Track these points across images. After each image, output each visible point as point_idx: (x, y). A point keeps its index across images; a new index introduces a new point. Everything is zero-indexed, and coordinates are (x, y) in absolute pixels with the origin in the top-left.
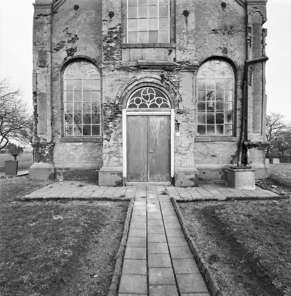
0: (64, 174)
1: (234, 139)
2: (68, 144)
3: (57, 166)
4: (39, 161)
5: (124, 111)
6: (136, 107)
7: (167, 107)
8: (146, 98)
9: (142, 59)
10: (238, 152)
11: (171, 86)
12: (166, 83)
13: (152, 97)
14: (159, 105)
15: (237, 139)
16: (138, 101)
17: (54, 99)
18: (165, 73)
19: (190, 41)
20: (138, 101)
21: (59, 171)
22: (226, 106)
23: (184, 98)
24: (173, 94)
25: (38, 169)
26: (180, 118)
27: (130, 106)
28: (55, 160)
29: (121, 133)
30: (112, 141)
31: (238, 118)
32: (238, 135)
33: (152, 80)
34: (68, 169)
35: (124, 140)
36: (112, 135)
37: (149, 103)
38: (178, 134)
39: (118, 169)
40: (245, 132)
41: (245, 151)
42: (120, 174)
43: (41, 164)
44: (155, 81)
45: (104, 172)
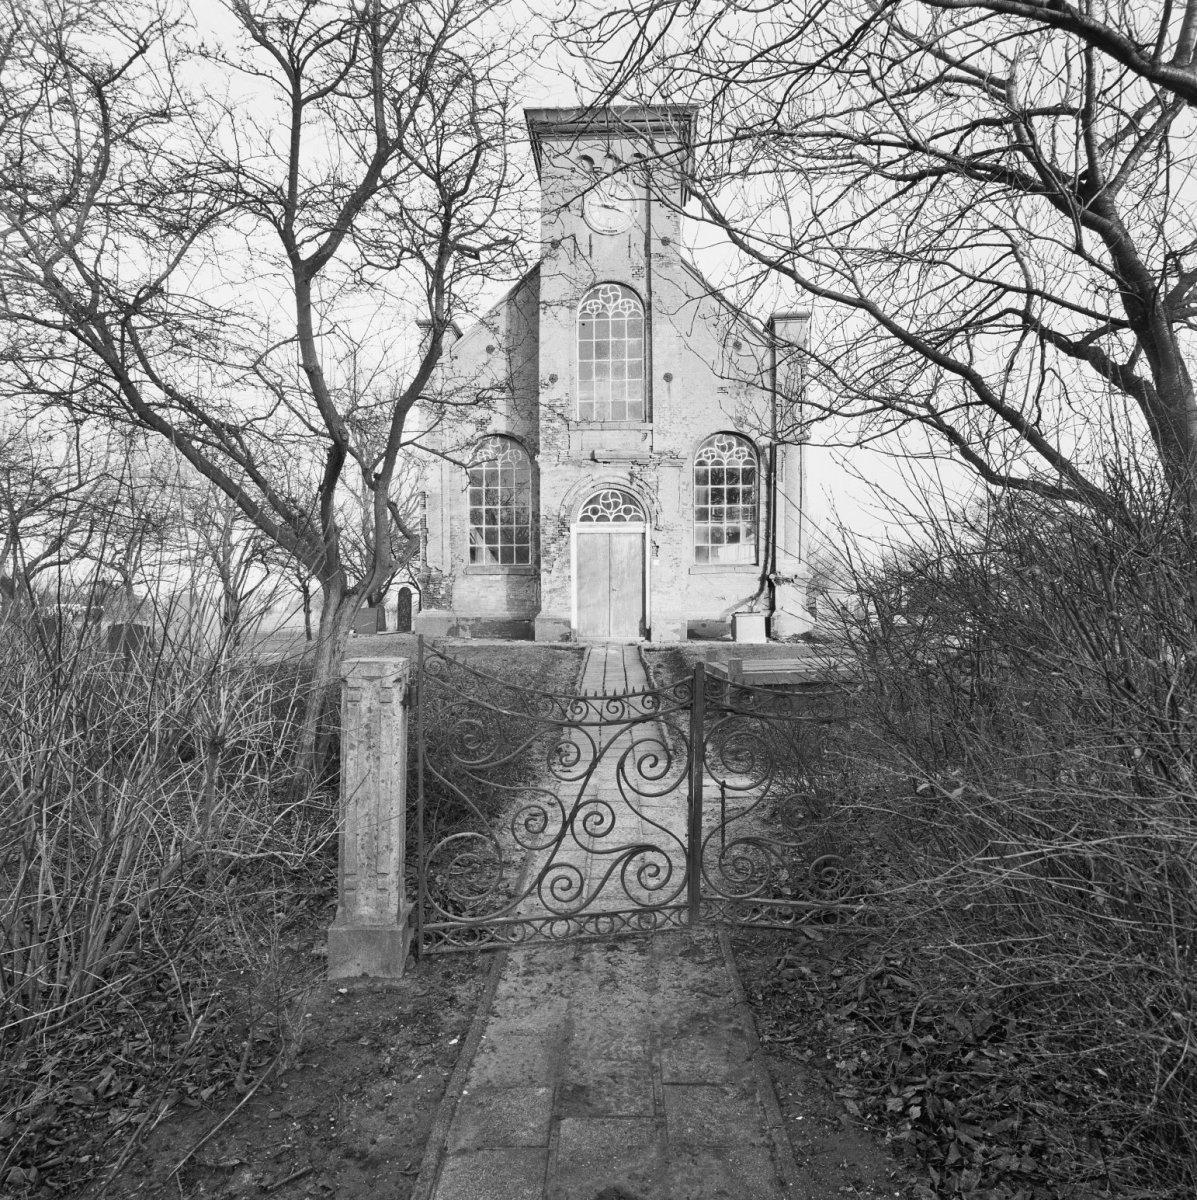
0: (471, 627)
1: (755, 568)
2: (478, 579)
3: (458, 614)
4: (429, 607)
5: (573, 527)
6: (591, 519)
7: (640, 519)
8: (608, 506)
9: (601, 448)
10: (761, 589)
11: (647, 490)
12: (549, 290)
13: (616, 504)
14: (627, 517)
15: (759, 570)
16: (595, 511)
17: (262, 471)
18: (637, 469)
19: (675, 420)
20: (595, 511)
21: (463, 623)
22: (349, 705)
23: (664, 508)
24: (648, 501)
25: (429, 620)
26: (660, 538)
27: (583, 519)
28: (455, 605)
29: (568, 561)
30: (554, 573)
31: (762, 534)
32: (761, 563)
33: (616, 480)
34: (478, 620)
35: (573, 571)
36: (556, 564)
37: (611, 513)
38: (656, 562)
39: (564, 616)
40: (254, 505)
41: (772, 587)
42: (568, 623)
43: (433, 612)
44: (622, 481)
45: (543, 621)
